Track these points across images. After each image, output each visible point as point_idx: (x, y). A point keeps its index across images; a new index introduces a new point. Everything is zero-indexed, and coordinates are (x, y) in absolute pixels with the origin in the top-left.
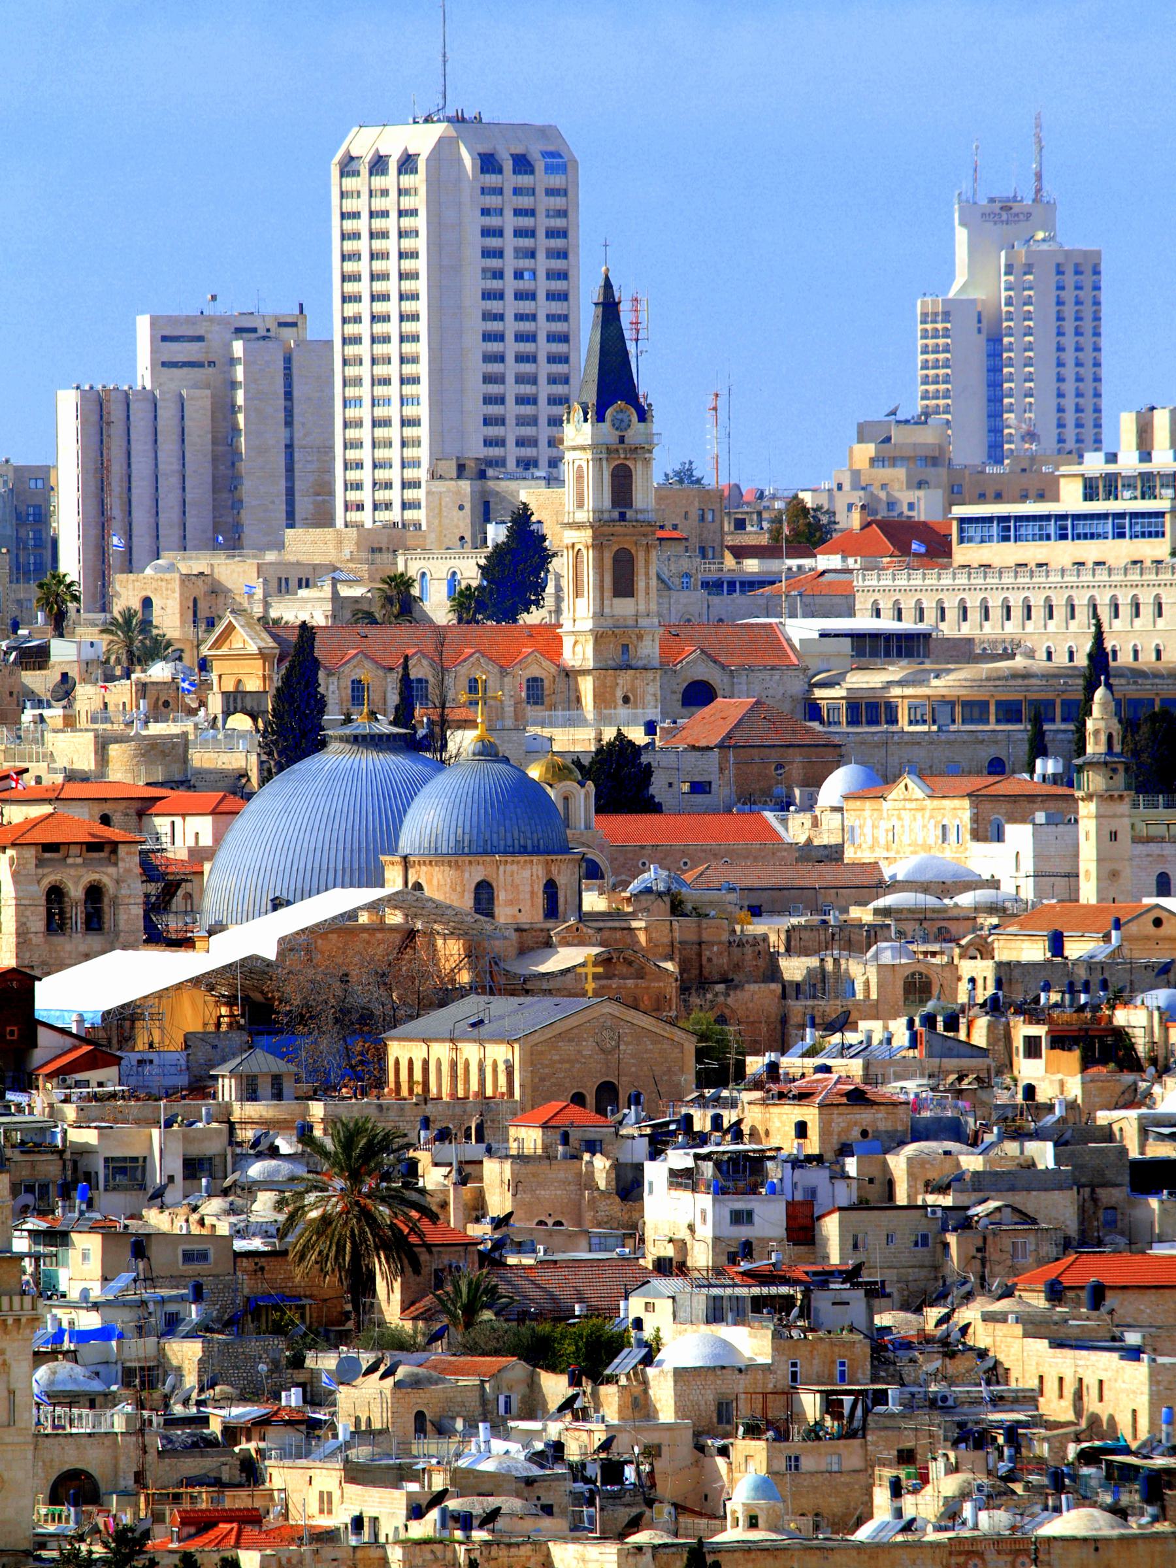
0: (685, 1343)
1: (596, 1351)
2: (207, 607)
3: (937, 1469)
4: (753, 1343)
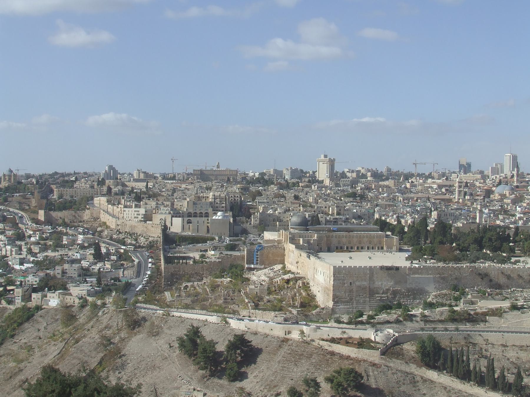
0: (518, 215)
1: (514, 215)
2: (496, 177)
3: (96, 271)
4: (522, 215)
